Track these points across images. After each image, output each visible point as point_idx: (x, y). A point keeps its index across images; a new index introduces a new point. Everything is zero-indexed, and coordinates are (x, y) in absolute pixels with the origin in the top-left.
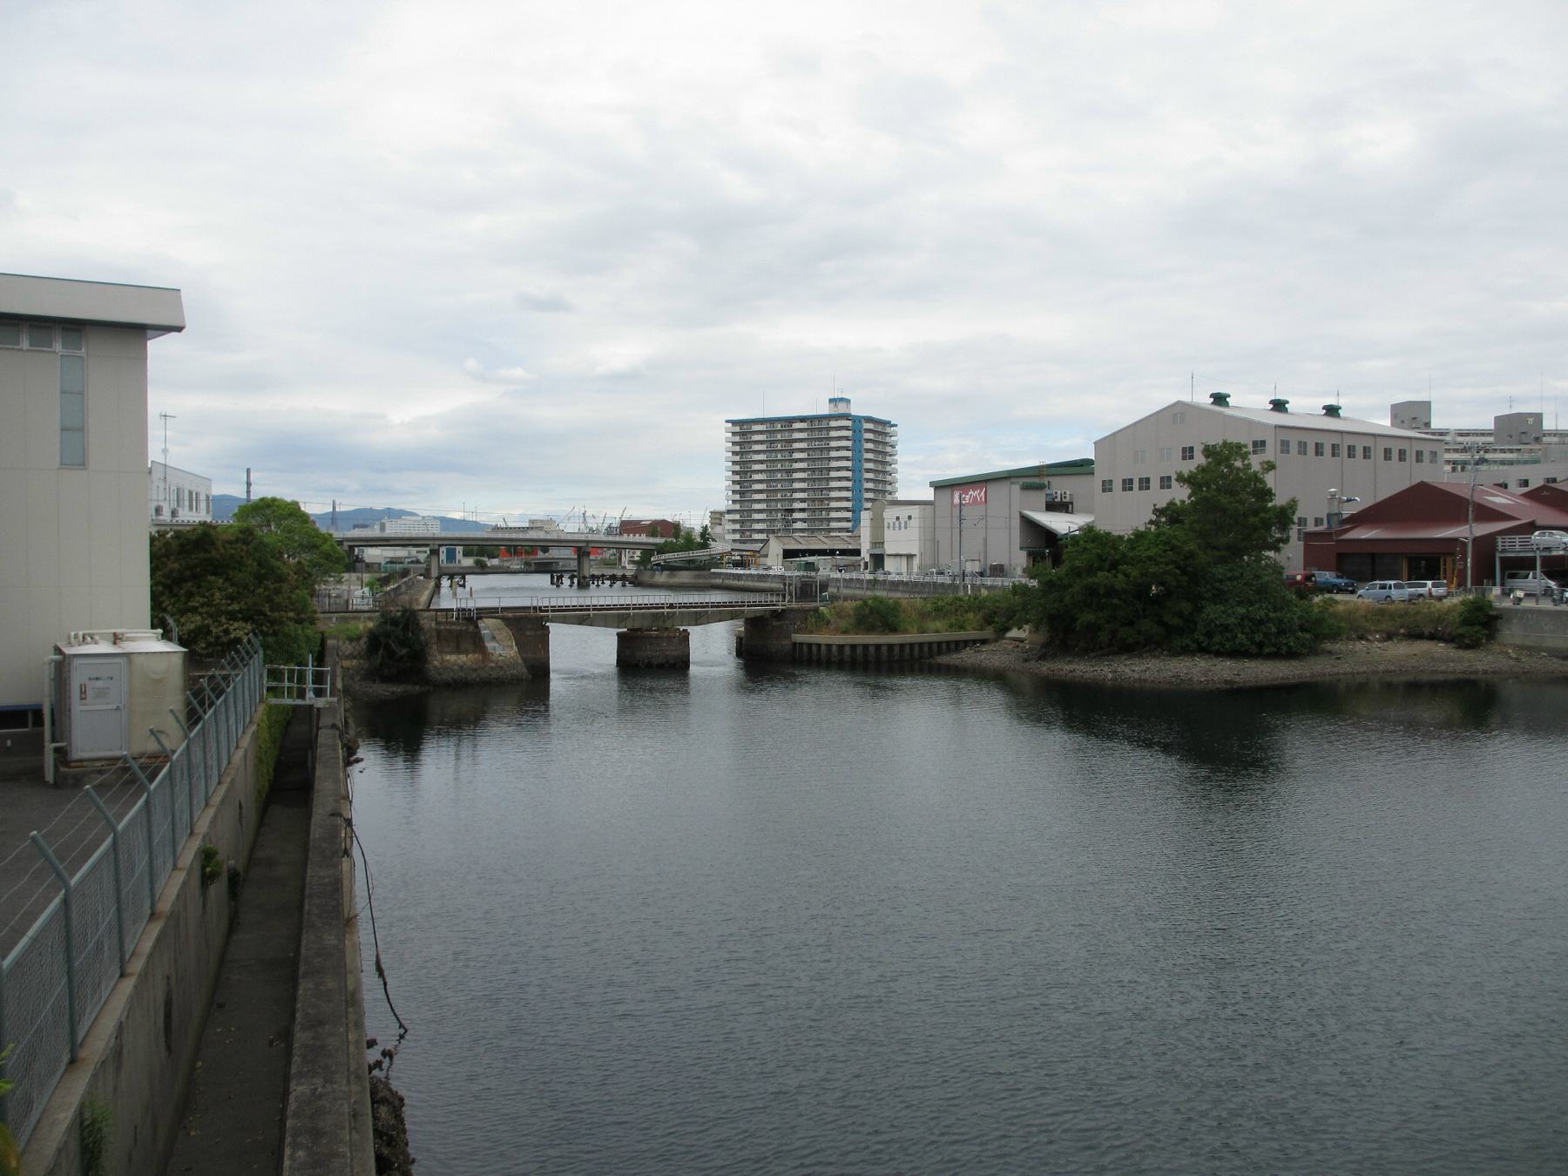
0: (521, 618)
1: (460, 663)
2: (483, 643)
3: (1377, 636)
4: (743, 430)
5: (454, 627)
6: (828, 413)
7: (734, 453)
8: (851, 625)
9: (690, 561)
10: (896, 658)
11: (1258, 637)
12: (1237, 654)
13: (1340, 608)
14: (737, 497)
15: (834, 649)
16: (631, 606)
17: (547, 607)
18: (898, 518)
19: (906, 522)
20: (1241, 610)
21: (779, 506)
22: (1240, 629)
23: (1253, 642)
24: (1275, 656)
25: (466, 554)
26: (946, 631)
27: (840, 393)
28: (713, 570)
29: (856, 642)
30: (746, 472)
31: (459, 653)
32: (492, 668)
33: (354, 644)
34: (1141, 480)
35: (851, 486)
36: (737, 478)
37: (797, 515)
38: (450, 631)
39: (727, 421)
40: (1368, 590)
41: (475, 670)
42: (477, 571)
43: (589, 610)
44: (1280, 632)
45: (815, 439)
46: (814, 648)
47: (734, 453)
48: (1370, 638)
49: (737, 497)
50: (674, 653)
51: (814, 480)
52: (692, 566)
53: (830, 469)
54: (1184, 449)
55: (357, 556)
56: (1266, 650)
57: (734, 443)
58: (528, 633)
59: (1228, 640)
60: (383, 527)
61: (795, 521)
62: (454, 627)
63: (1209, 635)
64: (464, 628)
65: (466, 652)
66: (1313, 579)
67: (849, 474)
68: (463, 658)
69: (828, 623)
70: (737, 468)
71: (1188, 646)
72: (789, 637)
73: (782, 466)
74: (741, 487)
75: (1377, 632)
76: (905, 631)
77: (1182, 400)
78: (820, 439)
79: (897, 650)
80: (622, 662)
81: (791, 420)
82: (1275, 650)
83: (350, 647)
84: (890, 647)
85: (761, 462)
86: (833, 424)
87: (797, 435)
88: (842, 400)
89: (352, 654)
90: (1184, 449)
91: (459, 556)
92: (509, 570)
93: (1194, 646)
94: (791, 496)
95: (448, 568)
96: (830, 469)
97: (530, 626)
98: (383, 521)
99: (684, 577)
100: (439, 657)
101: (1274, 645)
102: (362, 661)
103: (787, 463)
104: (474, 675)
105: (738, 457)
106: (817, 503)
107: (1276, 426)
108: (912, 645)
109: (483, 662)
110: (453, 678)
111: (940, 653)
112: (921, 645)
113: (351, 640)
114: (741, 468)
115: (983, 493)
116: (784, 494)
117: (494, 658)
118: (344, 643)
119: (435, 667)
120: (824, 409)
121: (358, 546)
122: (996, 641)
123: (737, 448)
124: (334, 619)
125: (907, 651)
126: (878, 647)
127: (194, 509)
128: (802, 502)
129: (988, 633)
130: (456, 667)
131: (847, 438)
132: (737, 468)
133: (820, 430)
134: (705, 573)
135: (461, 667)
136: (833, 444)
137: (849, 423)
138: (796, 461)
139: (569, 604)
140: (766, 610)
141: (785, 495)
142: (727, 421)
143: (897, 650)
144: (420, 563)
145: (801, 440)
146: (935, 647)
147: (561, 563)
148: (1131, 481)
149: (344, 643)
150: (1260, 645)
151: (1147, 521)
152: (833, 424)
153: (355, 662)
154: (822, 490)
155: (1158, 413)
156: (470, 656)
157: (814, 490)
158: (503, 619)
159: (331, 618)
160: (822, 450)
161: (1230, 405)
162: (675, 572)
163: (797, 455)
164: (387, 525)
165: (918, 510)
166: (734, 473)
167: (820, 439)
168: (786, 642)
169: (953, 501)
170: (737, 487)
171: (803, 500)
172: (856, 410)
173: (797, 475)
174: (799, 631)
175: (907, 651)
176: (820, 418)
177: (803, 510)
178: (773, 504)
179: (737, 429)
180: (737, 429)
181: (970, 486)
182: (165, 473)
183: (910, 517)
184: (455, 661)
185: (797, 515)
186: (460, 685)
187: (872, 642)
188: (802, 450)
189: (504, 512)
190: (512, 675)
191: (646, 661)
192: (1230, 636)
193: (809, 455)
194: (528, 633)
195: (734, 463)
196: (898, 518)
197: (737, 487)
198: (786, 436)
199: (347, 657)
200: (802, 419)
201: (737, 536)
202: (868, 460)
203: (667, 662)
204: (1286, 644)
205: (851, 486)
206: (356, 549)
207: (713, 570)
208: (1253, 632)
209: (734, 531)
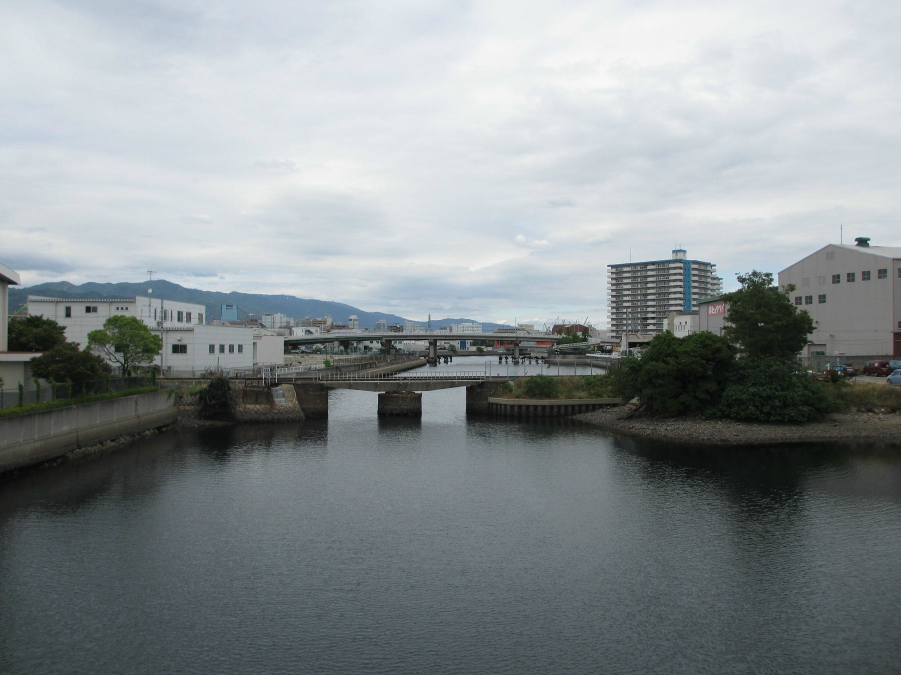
0: (306, 384)
1: (255, 409)
2: (273, 398)
3: (883, 410)
4: (618, 270)
5: (255, 389)
6: (672, 259)
7: (613, 285)
8: (522, 392)
9: (575, 349)
10: (547, 414)
11: (766, 409)
12: (749, 420)
13: (857, 389)
14: (614, 311)
15: (508, 407)
16: (401, 378)
17: (455, 377)
18: (680, 323)
19: (684, 326)
20: (751, 390)
21: (639, 316)
22: (752, 403)
23: (761, 412)
24: (780, 422)
25: (473, 344)
26: (588, 397)
27: (679, 247)
28: (587, 355)
29: (522, 403)
30: (619, 296)
31: (258, 404)
32: (275, 413)
33: (193, 397)
34: (807, 297)
35: (682, 303)
36: (614, 299)
37: (649, 321)
38: (253, 391)
39: (608, 266)
40: (893, 375)
41: (265, 414)
42: (477, 354)
43: (400, 380)
44: (785, 405)
45: (661, 275)
46: (499, 406)
47: (613, 285)
48: (876, 411)
49: (614, 311)
50: (406, 407)
51: (660, 300)
52: (576, 352)
53: (670, 293)
54: (834, 276)
55: (393, 346)
56: (772, 418)
57: (612, 279)
58: (311, 393)
59: (742, 410)
60: (451, 330)
61: (649, 325)
62: (255, 389)
63: (730, 406)
64: (262, 390)
65: (260, 404)
66: (887, 366)
67: (681, 296)
68: (258, 407)
69: (511, 391)
70: (614, 293)
71: (715, 414)
72: (487, 399)
73: (640, 292)
74: (616, 305)
75: (883, 407)
76: (556, 397)
77: (832, 243)
78: (663, 275)
79: (548, 410)
80: (381, 414)
81: (646, 264)
82: (780, 418)
83: (190, 399)
84: (544, 407)
85: (628, 290)
86: (672, 265)
87: (650, 273)
88: (680, 251)
89: (191, 402)
90: (834, 276)
91: (468, 345)
92: (497, 353)
93: (719, 414)
94: (646, 310)
95: (461, 352)
96: (670, 293)
97: (312, 389)
98: (451, 325)
99: (571, 358)
100: (243, 406)
101: (780, 415)
102: (196, 407)
103: (644, 290)
104: (263, 417)
105: (615, 287)
106: (662, 314)
107: (894, 259)
108: (559, 407)
109: (270, 409)
110: (250, 418)
111: (580, 412)
112: (566, 406)
113: (192, 395)
114: (616, 293)
115: (723, 308)
116: (642, 308)
117: (277, 407)
118: (187, 396)
119: (240, 411)
120: (670, 257)
121: (438, 340)
122: (624, 405)
123: (614, 282)
124: (194, 383)
125: (555, 410)
126: (536, 407)
127: (185, 319)
128: (653, 313)
129: (618, 400)
130: (252, 412)
131: (680, 274)
132: (614, 293)
133: (664, 269)
134: (583, 356)
135: (256, 412)
136: (672, 278)
137: (681, 265)
138: (649, 288)
139: (438, 376)
140: (475, 382)
141: (643, 309)
142: (608, 266)
143: (548, 410)
144: (446, 349)
145: (652, 276)
146: (577, 408)
147: (529, 350)
148: (800, 298)
149: (187, 396)
150: (769, 414)
151: (722, 327)
152: (672, 265)
153: (192, 407)
154: (665, 306)
155: (817, 252)
156: (262, 406)
157: (660, 306)
158: (294, 384)
159: (192, 382)
160: (665, 281)
161: (870, 245)
162: (566, 356)
163: (650, 285)
164: (453, 328)
165: (689, 318)
166: (613, 296)
167: (663, 275)
168: (484, 402)
169: (708, 312)
170: (614, 305)
171: (653, 312)
172: (689, 257)
173: (649, 297)
174: (493, 395)
175: (555, 410)
176: (664, 262)
177: (653, 318)
178: (636, 314)
179: (614, 270)
180: (614, 270)
181: (717, 303)
182: (150, 302)
183: (686, 323)
184: (253, 408)
185: (649, 321)
186: (254, 422)
187: (531, 404)
188: (652, 282)
189: (563, 318)
190: (288, 418)
191: (390, 412)
192: (744, 408)
193: (657, 285)
194: (311, 393)
195: (613, 290)
196: (680, 323)
197: (614, 305)
198: (643, 274)
199: (188, 405)
200: (653, 263)
201: (614, 334)
202: (695, 287)
203: (402, 412)
204: (789, 414)
205: (682, 303)
206: (393, 342)
207: (587, 355)
208: (763, 405)
209: (613, 331)
